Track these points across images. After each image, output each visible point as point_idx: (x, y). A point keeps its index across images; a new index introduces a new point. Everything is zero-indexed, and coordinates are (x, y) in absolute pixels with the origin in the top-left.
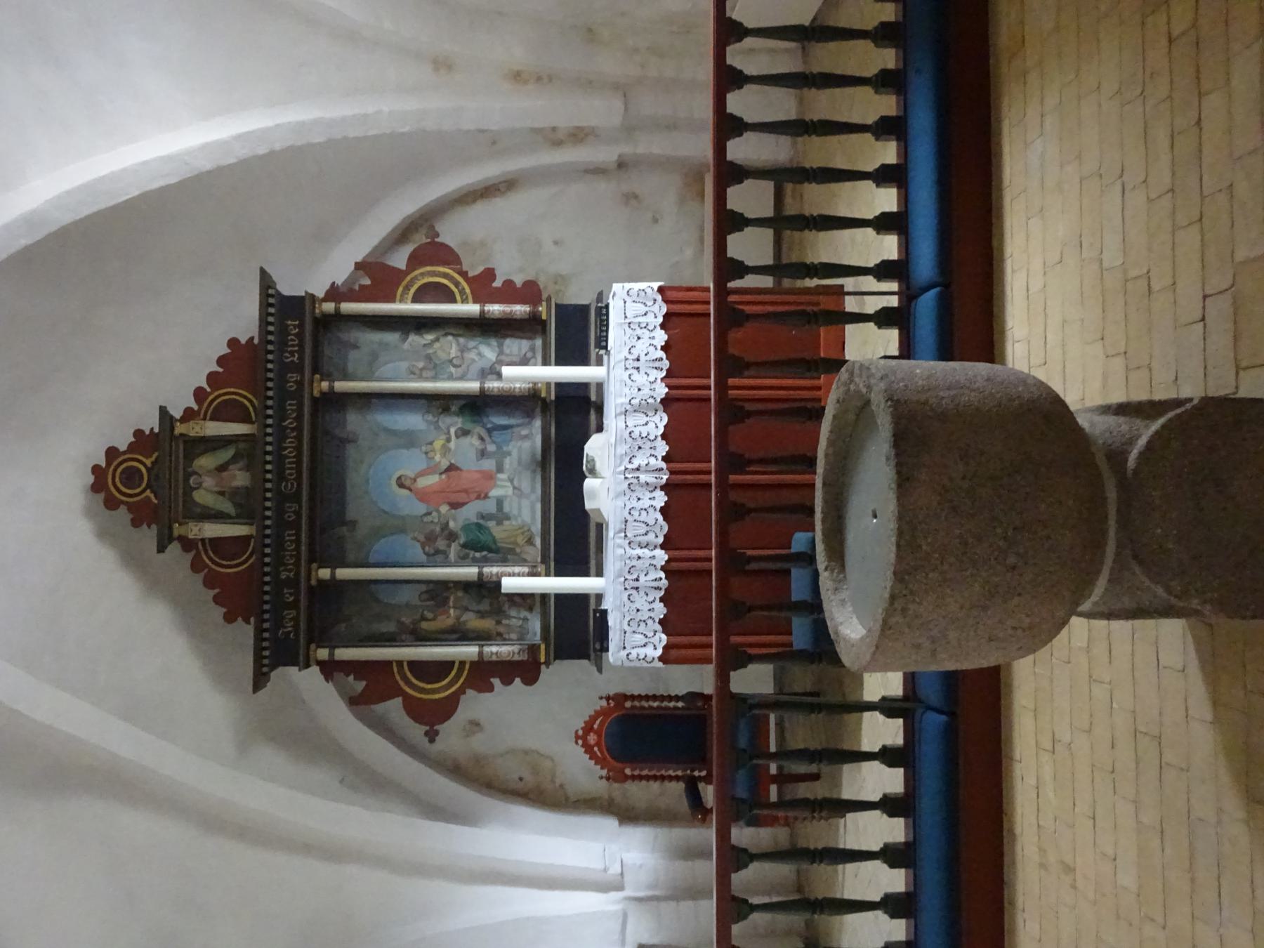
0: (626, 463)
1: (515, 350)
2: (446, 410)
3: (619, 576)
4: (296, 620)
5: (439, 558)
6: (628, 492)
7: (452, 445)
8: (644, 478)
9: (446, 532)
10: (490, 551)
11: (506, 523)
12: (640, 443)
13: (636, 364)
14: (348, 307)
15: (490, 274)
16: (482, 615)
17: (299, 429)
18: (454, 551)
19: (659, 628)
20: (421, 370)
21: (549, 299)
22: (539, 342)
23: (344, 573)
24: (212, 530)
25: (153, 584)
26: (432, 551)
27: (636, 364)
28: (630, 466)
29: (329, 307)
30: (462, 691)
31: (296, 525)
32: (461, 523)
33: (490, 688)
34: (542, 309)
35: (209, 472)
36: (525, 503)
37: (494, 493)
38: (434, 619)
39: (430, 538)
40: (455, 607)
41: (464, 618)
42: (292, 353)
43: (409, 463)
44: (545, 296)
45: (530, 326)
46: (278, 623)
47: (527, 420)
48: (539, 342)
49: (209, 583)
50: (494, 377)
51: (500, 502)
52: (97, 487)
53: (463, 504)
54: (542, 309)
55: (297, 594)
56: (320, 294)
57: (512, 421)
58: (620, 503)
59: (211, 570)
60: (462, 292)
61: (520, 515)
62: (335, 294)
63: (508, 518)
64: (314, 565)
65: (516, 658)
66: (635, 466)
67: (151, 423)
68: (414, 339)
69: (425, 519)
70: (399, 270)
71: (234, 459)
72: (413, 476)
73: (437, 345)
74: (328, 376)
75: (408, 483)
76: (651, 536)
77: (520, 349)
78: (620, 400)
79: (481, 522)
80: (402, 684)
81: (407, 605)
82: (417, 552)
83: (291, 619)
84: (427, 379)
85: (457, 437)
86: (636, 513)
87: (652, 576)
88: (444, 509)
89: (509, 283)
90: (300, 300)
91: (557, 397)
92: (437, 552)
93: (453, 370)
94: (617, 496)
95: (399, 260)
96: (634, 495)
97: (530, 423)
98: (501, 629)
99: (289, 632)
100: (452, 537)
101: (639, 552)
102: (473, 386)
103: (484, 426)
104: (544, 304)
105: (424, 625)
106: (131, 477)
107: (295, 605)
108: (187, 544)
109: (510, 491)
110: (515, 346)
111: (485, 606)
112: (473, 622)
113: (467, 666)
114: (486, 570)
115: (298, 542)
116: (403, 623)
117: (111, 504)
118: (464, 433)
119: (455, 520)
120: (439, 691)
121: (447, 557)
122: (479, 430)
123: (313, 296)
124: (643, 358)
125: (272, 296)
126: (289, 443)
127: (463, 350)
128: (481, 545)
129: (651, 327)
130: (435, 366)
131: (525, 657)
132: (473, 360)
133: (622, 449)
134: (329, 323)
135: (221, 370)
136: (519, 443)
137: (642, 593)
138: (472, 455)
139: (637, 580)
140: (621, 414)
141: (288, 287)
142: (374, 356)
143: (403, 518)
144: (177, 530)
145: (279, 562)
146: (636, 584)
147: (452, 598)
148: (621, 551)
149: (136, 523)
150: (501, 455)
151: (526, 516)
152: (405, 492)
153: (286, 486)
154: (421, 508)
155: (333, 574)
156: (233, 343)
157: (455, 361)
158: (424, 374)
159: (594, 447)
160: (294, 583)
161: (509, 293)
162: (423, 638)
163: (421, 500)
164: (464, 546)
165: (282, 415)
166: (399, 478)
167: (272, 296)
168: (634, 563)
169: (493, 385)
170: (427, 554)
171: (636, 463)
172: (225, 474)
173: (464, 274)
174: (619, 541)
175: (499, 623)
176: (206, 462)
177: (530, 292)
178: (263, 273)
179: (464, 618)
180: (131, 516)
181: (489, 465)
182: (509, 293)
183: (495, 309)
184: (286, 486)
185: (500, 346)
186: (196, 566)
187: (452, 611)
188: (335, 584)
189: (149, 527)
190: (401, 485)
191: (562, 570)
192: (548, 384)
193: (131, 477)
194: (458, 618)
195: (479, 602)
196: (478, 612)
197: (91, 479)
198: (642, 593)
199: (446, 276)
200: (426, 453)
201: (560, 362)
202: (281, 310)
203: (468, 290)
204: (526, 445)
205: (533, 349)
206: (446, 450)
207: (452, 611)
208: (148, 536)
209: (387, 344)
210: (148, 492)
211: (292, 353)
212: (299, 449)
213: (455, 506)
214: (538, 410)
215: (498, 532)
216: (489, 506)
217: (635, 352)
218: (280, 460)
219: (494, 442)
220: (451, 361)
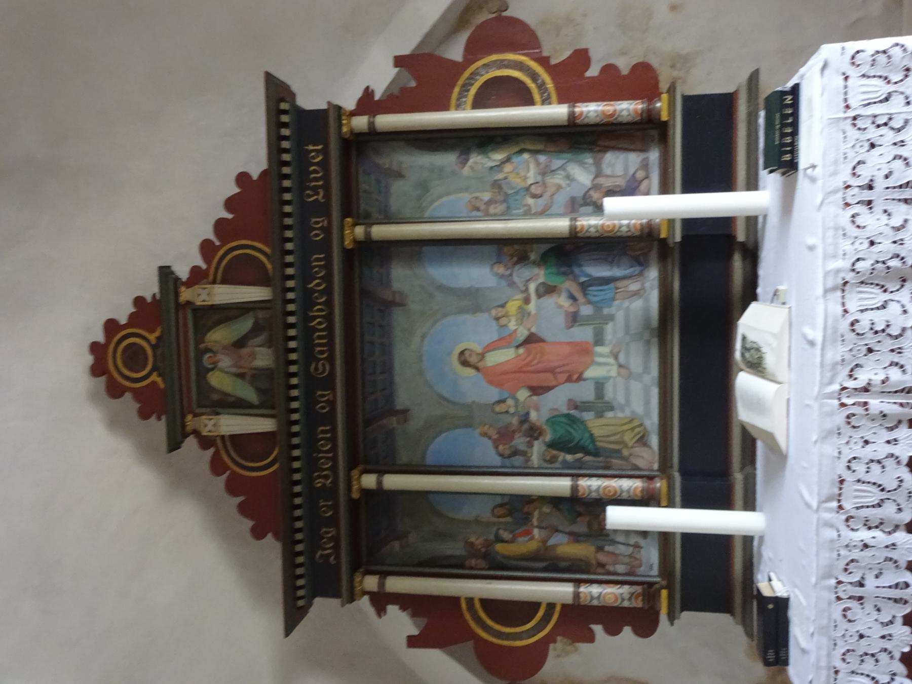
0: (842, 378)
1: (619, 170)
2: (522, 259)
3: (827, 576)
4: (336, 539)
5: (518, 460)
6: (847, 431)
7: (532, 307)
8: (876, 404)
9: (526, 426)
10: (587, 453)
11: (610, 414)
12: (871, 340)
13: (867, 195)
14: (387, 121)
15: (581, 57)
16: (576, 538)
17: (329, 291)
18: (537, 451)
19: (901, 668)
20: (489, 203)
21: (671, 90)
22: (654, 155)
23: (393, 481)
24: (231, 424)
25: (177, 482)
26: (507, 452)
27: (867, 195)
28: (851, 384)
29: (360, 123)
30: (549, 639)
31: (330, 418)
32: (545, 415)
33: (590, 638)
34: (661, 105)
35: (225, 348)
36: (636, 387)
37: (592, 373)
38: (512, 541)
39: (504, 435)
40: (539, 527)
41: (551, 542)
42: (315, 189)
43: (475, 332)
44: (664, 86)
45: (645, 131)
46: (314, 542)
47: (638, 269)
48: (654, 155)
49: (232, 488)
50: (590, 209)
51: (600, 386)
52: (97, 370)
53: (548, 389)
54: (661, 105)
55: (335, 507)
56: (349, 103)
57: (617, 272)
58: (830, 449)
59: (234, 473)
60: (542, 87)
61: (628, 403)
62: (368, 104)
63: (612, 408)
64: (355, 473)
65: (626, 604)
66: (860, 383)
67: (150, 288)
68: (478, 161)
69: (498, 408)
70: (454, 63)
71: (256, 329)
72: (479, 350)
73: (508, 168)
74: (367, 220)
75: (473, 360)
76: (889, 510)
77: (626, 168)
78: (834, 265)
79: (573, 412)
80: (472, 624)
81: (477, 521)
82: (487, 453)
83: (330, 539)
84: (496, 218)
85: (539, 296)
86: (860, 468)
87: (891, 577)
88: (523, 394)
89: (609, 69)
90: (320, 116)
91: (683, 237)
92: (515, 453)
93: (530, 201)
94: (826, 436)
95: (455, 52)
96: (857, 435)
97: (641, 274)
98: (602, 557)
99: (329, 555)
100: (534, 432)
101: (865, 535)
102: (559, 225)
103: (575, 278)
104: (665, 96)
105: (500, 547)
106: (134, 357)
107: (334, 521)
108: (206, 442)
109: (614, 371)
110: (619, 163)
111: (581, 527)
112: (565, 547)
113: (558, 609)
114: (584, 483)
115: (333, 440)
116: (472, 544)
117: (114, 391)
118: (547, 290)
119: (537, 409)
120: (521, 637)
121: (528, 460)
122: (568, 285)
123: (339, 108)
124: (880, 184)
125: (285, 112)
126: (317, 311)
127: (545, 172)
128: (574, 445)
129: (896, 124)
130: (507, 196)
131: (639, 604)
132: (559, 187)
133: (837, 353)
134: (360, 146)
135: (230, 216)
136: (626, 303)
137: (869, 607)
138: (560, 320)
139: (861, 585)
140: (834, 289)
141: (309, 101)
142: (424, 187)
143: (469, 407)
144: (191, 422)
145: (312, 465)
146: (858, 592)
147: (536, 514)
148: (831, 534)
149: (144, 414)
150: (600, 321)
151: (638, 407)
152: (469, 372)
153: (316, 369)
154: (492, 394)
155: (379, 483)
156: (242, 178)
157: (533, 189)
158: (492, 210)
159: (755, 323)
160: (331, 493)
161: (611, 84)
162: (500, 568)
163: (491, 382)
164: (552, 445)
165: (306, 275)
166: (462, 353)
167: (285, 112)
168: (856, 554)
169: (589, 222)
170: (501, 455)
171: (863, 377)
172: (245, 351)
173: (544, 61)
174: (827, 516)
175: (600, 549)
176: (219, 336)
177: (642, 81)
178: (270, 80)
179: (551, 542)
180: (138, 406)
181: (583, 334)
182: (611, 84)
183: (591, 110)
184: (316, 369)
185: (598, 164)
186: (217, 467)
187: (536, 532)
188: (378, 495)
189: (159, 419)
190: (465, 363)
191: (693, 499)
192: (671, 222)
193: (134, 357)
194: (544, 542)
195: (573, 522)
196: (570, 534)
197: (89, 359)
198: (869, 607)
199: (520, 66)
200: (497, 319)
201: (688, 188)
202: (295, 126)
203: (550, 85)
204: (637, 305)
205: (645, 166)
206: (523, 314)
207: (536, 532)
208: (158, 428)
209: (441, 169)
210: (155, 377)
211: (315, 189)
212: (329, 318)
213: (537, 390)
214: (654, 255)
215: (598, 427)
216: (585, 392)
217: (865, 173)
218: (308, 333)
219: (590, 302)
220: (528, 189)
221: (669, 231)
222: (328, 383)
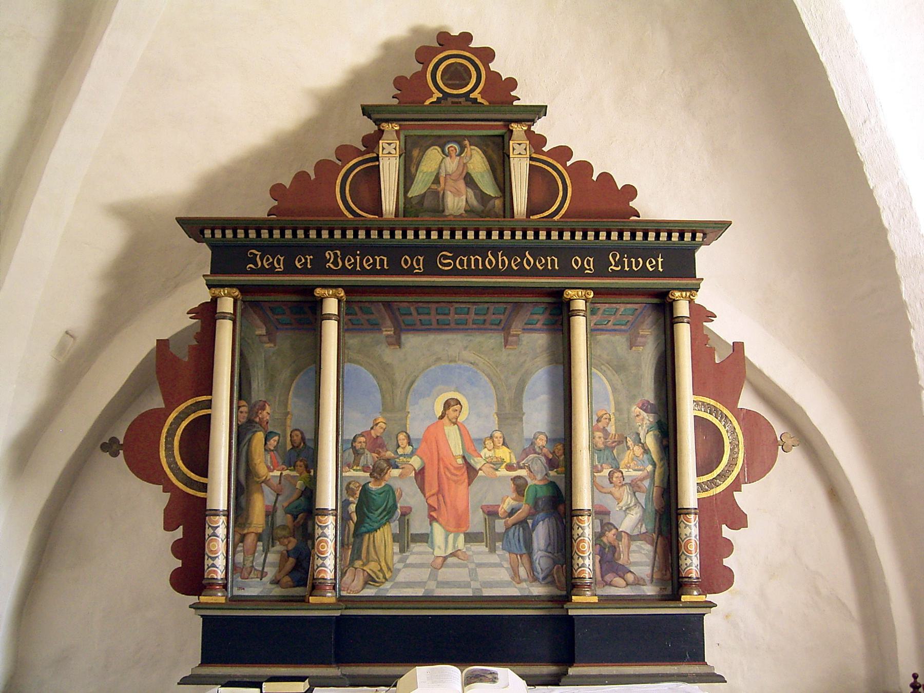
14: (684, 333)
15: (739, 520)
16: (270, 514)
17: (521, 272)
23: (331, 330)
29: (683, 309)
30: (168, 487)
43: (479, 414)
48: (650, 590)
51: (425, 538)
71: (483, 198)
82: (356, 426)
100: (377, 472)
102: (584, 499)
107: (290, 269)
118: (520, 486)
127: (634, 486)
150: (488, 538)
154: (416, 429)
177: (718, 578)
181: (477, 522)
182: (715, 548)
183: (691, 530)
204: (504, 575)
215: (384, 535)
222: (431, 269)
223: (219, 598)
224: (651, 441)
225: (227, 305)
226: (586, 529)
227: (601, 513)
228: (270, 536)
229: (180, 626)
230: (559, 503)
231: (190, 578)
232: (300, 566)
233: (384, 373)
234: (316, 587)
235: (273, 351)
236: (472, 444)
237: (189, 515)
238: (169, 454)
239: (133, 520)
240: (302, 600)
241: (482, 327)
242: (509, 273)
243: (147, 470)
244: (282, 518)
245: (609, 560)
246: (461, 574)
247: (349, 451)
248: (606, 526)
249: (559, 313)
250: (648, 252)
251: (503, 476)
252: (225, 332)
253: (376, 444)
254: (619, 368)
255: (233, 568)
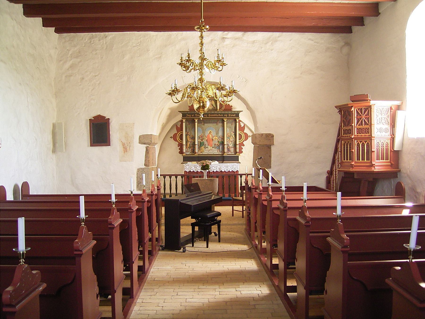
14: (238, 124)
15: (244, 145)
16: (190, 145)
17: (219, 117)
23: (196, 123)
29: (237, 121)
30: (178, 142)
43: (214, 133)
48: (233, 153)
51: (207, 147)
71: (214, 107)
82: (200, 135)
100: (202, 140)
102: (225, 143)
107: (191, 117)
118: (218, 141)
127: (232, 141)
150: (215, 148)
154: (206, 135)
177: (241, 152)
181: (213, 146)
182: (241, 149)
183: (238, 146)
204: (217, 152)
215: (203, 147)
221: (175, 116)
222: (208, 116)
223: (185, 154)
224: (234, 136)
225: (184, 121)
226: (226, 146)
227: (228, 145)
228: (190, 147)
229: (181, 157)
230: (223, 143)
231: (181, 152)
232: (193, 151)
233: (202, 128)
234: (195, 153)
235: (190, 126)
236: (213, 137)
237: (181, 145)
238: (178, 138)
239: (173, 146)
240: (194, 155)
241: (214, 123)
242: (217, 117)
243: (175, 140)
244: (191, 145)
245: (228, 150)
246: (212, 152)
247: (199, 138)
248: (228, 146)
249: (223, 121)
250: (234, 114)
251: (216, 140)
252: (184, 124)
253: (202, 137)
254: (230, 128)
255: (186, 151)
